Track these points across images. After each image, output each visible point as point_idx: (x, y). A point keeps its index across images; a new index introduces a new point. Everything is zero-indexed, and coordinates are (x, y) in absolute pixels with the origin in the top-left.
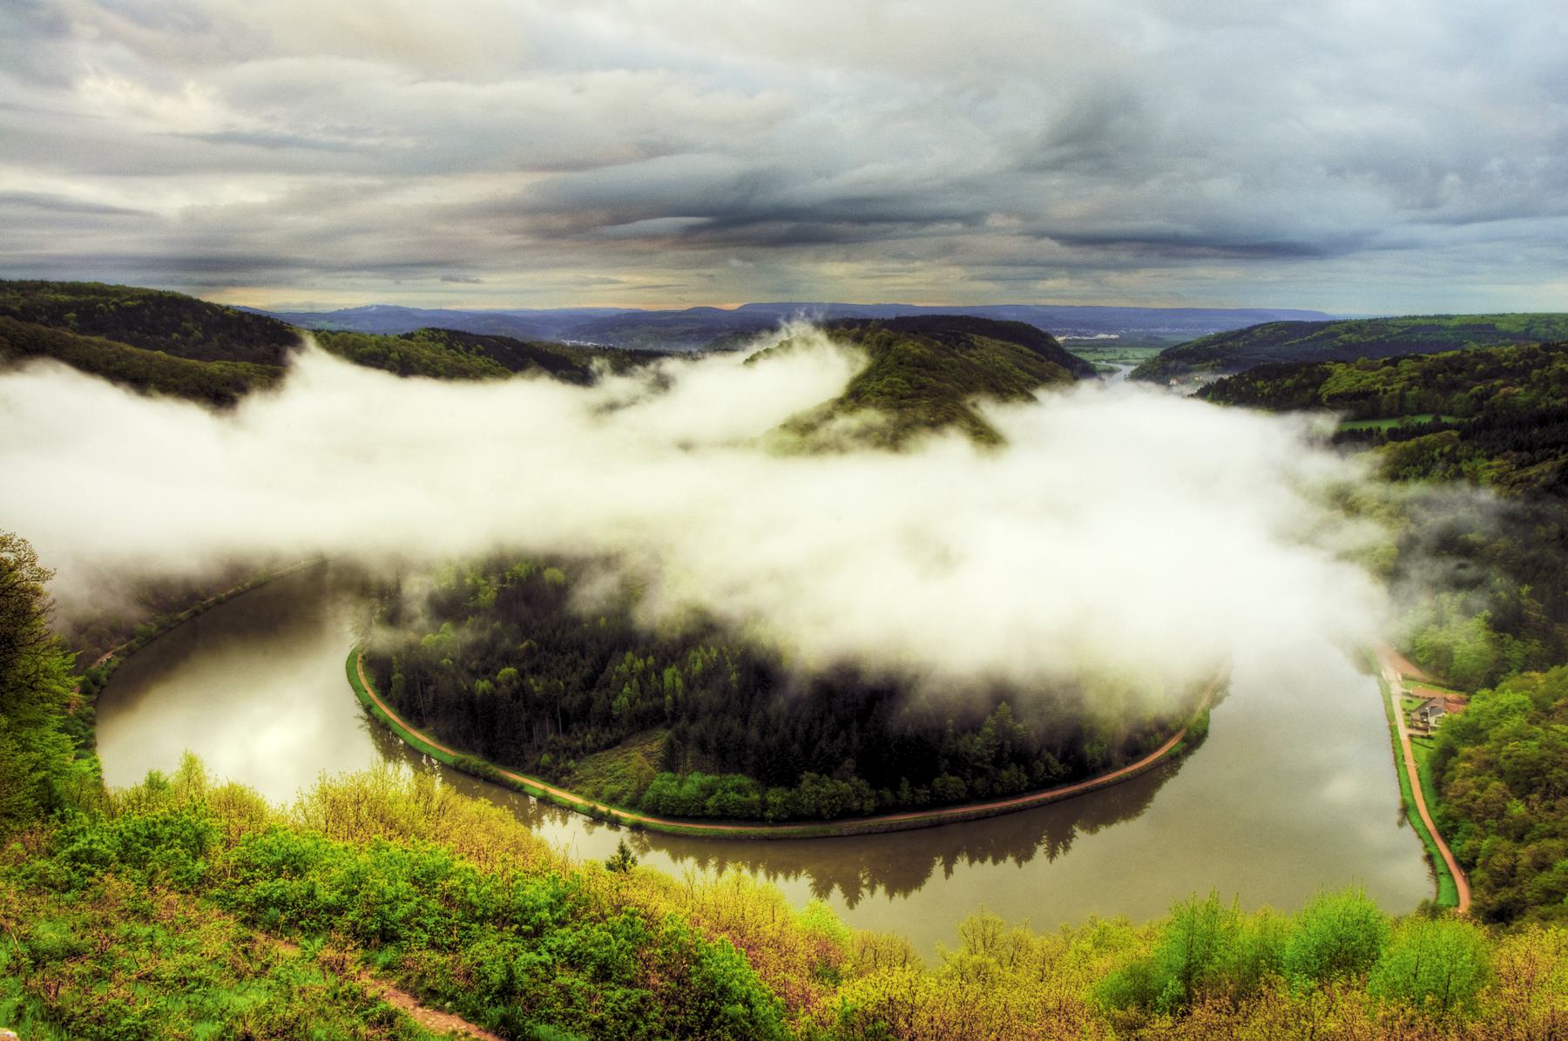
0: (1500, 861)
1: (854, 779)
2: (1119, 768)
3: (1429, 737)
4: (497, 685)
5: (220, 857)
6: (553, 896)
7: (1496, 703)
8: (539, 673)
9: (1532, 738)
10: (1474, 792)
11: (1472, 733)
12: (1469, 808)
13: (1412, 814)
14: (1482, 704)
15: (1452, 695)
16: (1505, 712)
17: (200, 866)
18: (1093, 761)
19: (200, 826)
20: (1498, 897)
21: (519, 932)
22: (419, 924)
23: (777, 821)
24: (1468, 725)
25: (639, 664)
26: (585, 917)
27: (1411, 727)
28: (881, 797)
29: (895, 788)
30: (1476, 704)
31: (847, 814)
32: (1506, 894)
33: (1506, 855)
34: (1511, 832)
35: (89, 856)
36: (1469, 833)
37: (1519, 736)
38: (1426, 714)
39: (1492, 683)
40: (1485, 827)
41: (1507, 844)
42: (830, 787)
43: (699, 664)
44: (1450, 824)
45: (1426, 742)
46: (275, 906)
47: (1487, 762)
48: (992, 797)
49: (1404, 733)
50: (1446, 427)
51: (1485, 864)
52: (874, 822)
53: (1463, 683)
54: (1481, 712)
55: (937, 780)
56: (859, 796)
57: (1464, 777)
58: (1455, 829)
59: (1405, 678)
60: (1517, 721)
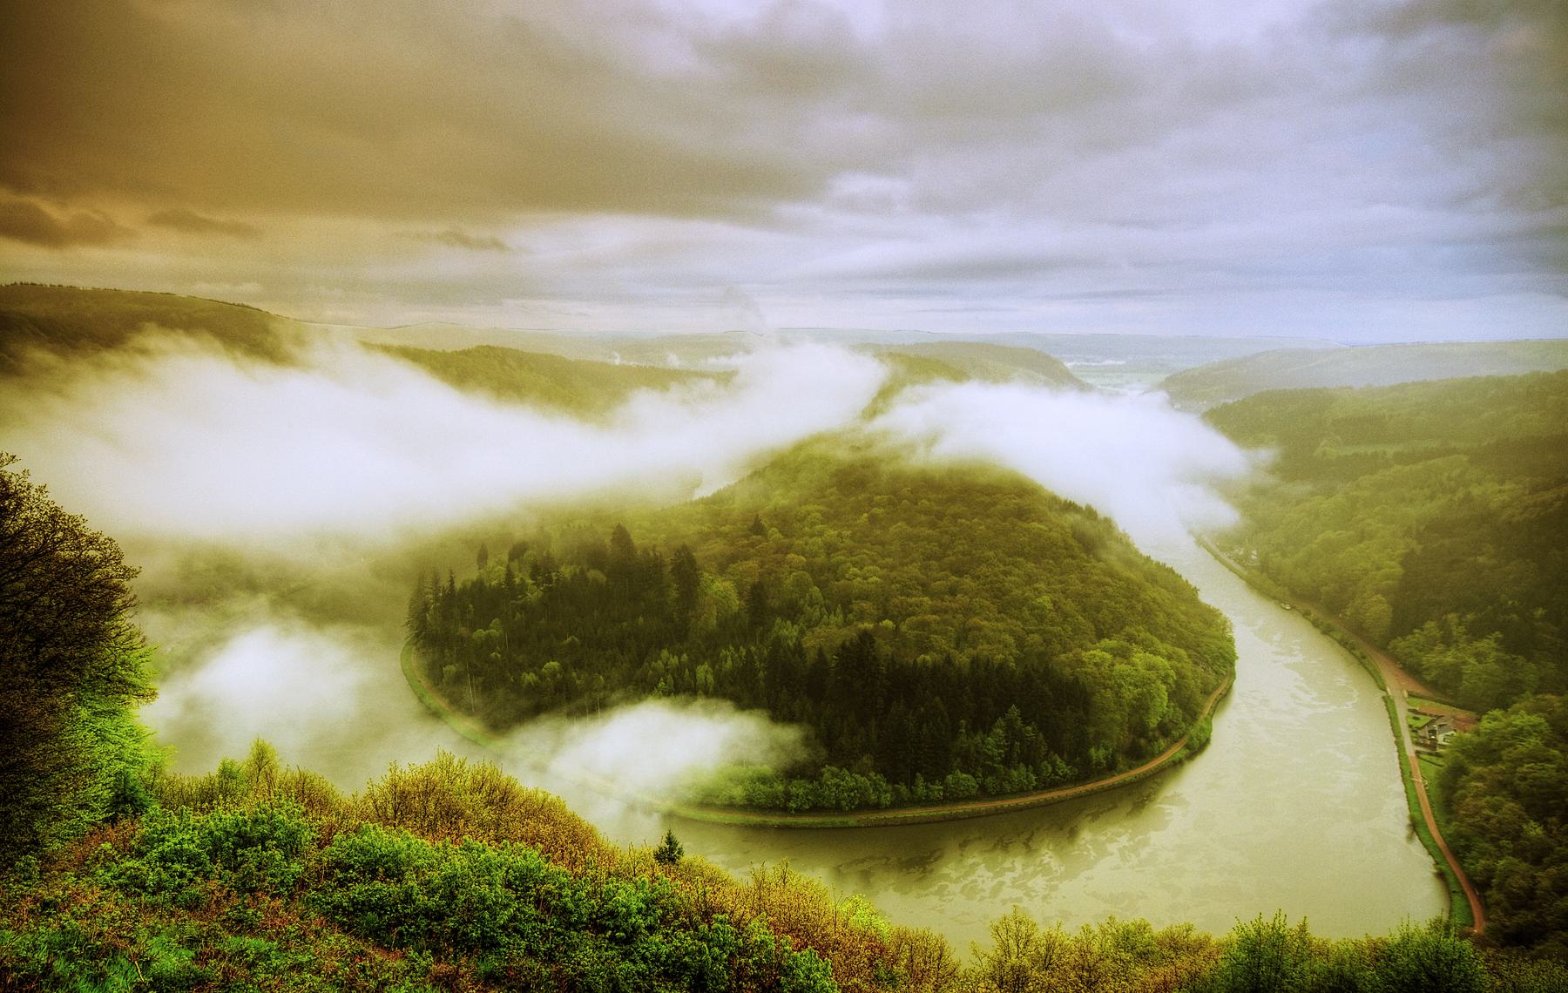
0: (1517, 882)
1: (872, 774)
2: (1121, 772)
3: (1438, 755)
4: (542, 678)
5: (314, 857)
6: (643, 901)
7: (1510, 725)
8: (581, 668)
9: (1549, 761)
10: (1486, 812)
11: (1487, 752)
12: (1482, 827)
13: (1420, 830)
14: (1494, 724)
15: (1462, 714)
16: (1519, 733)
17: (296, 867)
18: (1099, 764)
19: (292, 825)
20: (1516, 919)
21: (612, 938)
22: (516, 930)
23: (799, 811)
24: (1481, 744)
25: (674, 661)
26: (676, 923)
27: (1417, 744)
28: (897, 792)
29: (911, 783)
30: (1486, 724)
31: (865, 806)
32: (1524, 917)
33: (1523, 878)
34: (1528, 855)
35: (178, 854)
36: (1483, 854)
37: (1533, 757)
38: (1433, 732)
39: (1503, 704)
40: (1500, 848)
41: (1524, 866)
42: (850, 780)
43: (729, 662)
44: (1463, 842)
45: (1434, 759)
46: (372, 910)
47: (1500, 782)
48: (1001, 794)
49: (1410, 749)
50: (1455, 451)
51: (1500, 887)
52: (890, 815)
53: (1476, 706)
54: (1493, 732)
55: (950, 777)
56: (876, 789)
57: (1476, 796)
58: (1468, 848)
59: (1411, 695)
60: (1533, 742)
